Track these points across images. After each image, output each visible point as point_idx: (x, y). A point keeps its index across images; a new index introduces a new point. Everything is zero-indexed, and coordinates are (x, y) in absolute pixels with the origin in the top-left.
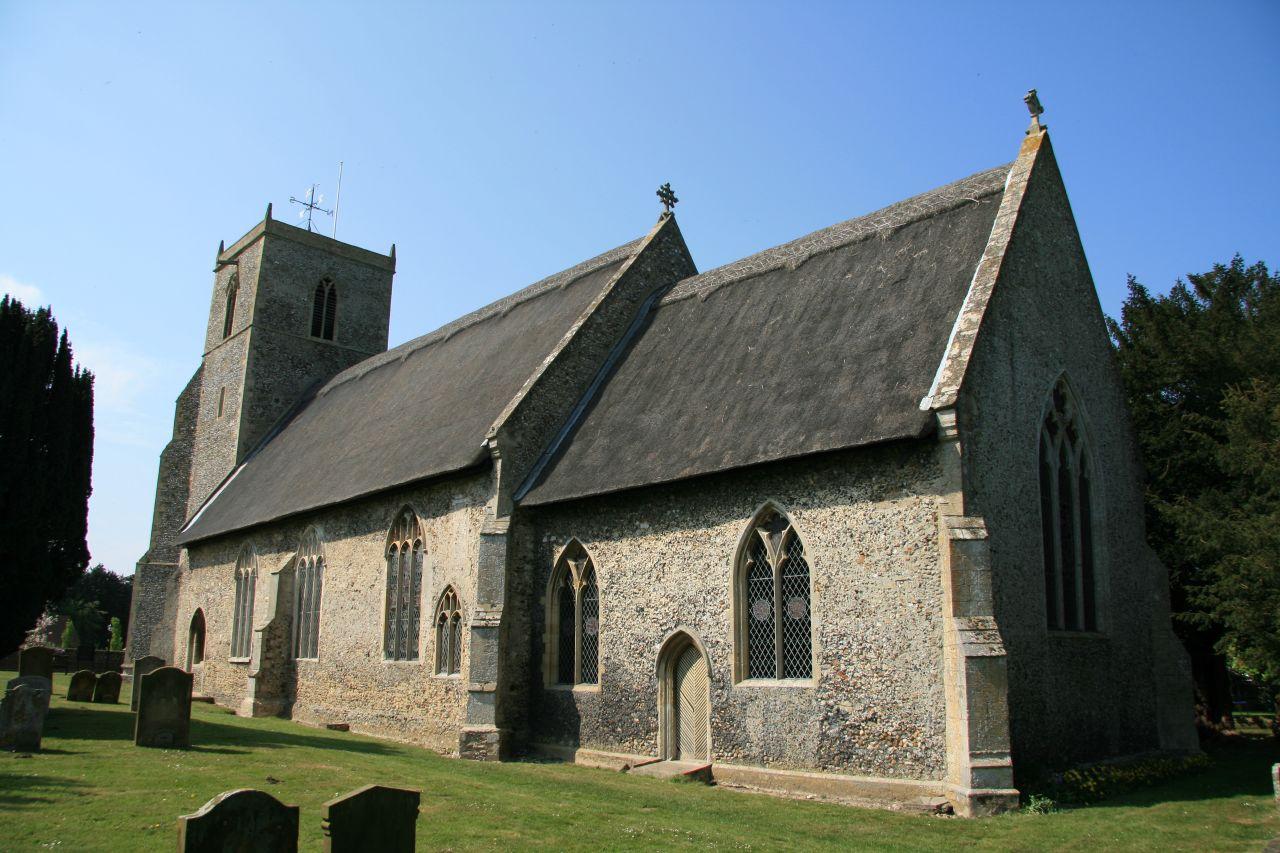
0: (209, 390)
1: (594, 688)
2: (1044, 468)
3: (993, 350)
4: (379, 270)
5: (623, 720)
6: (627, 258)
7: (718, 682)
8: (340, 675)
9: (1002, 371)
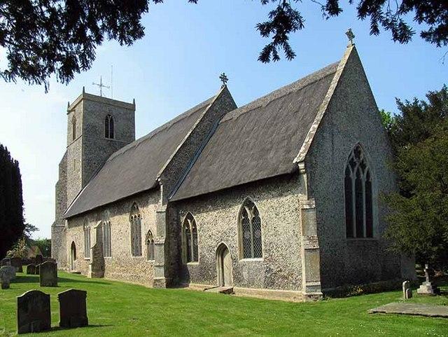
0: (70, 159)
1: (198, 263)
2: (348, 180)
3: (323, 138)
4: (130, 108)
5: (206, 274)
6: (209, 105)
7: (234, 260)
8: (119, 262)
9: (328, 145)
